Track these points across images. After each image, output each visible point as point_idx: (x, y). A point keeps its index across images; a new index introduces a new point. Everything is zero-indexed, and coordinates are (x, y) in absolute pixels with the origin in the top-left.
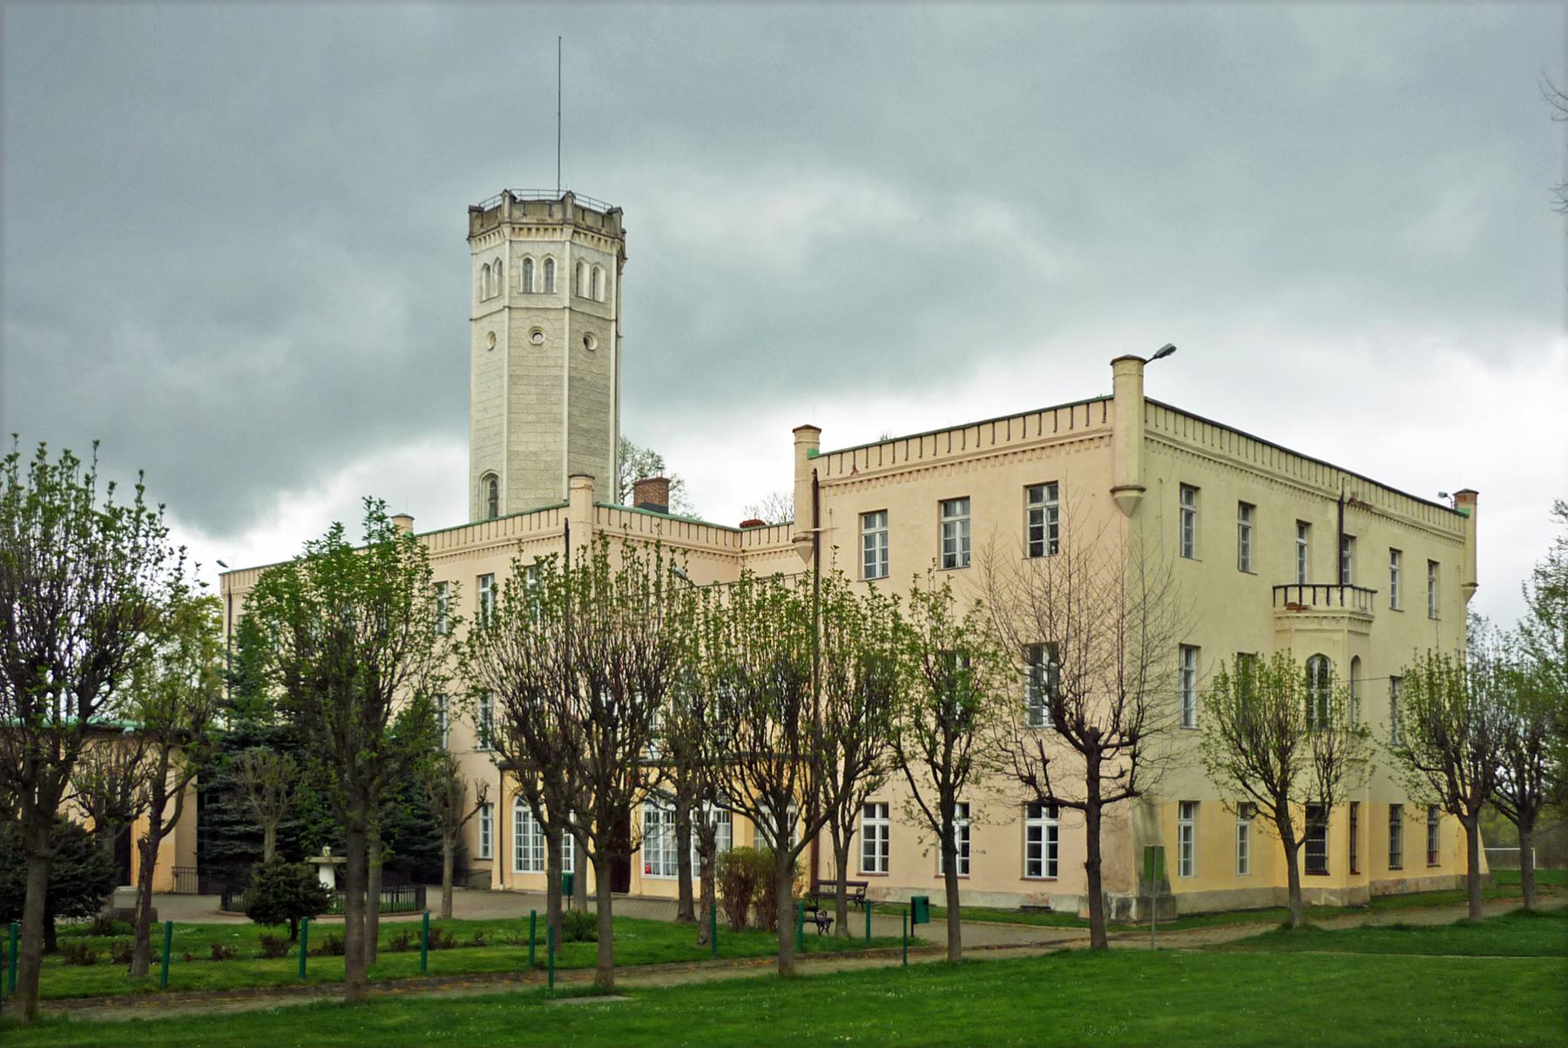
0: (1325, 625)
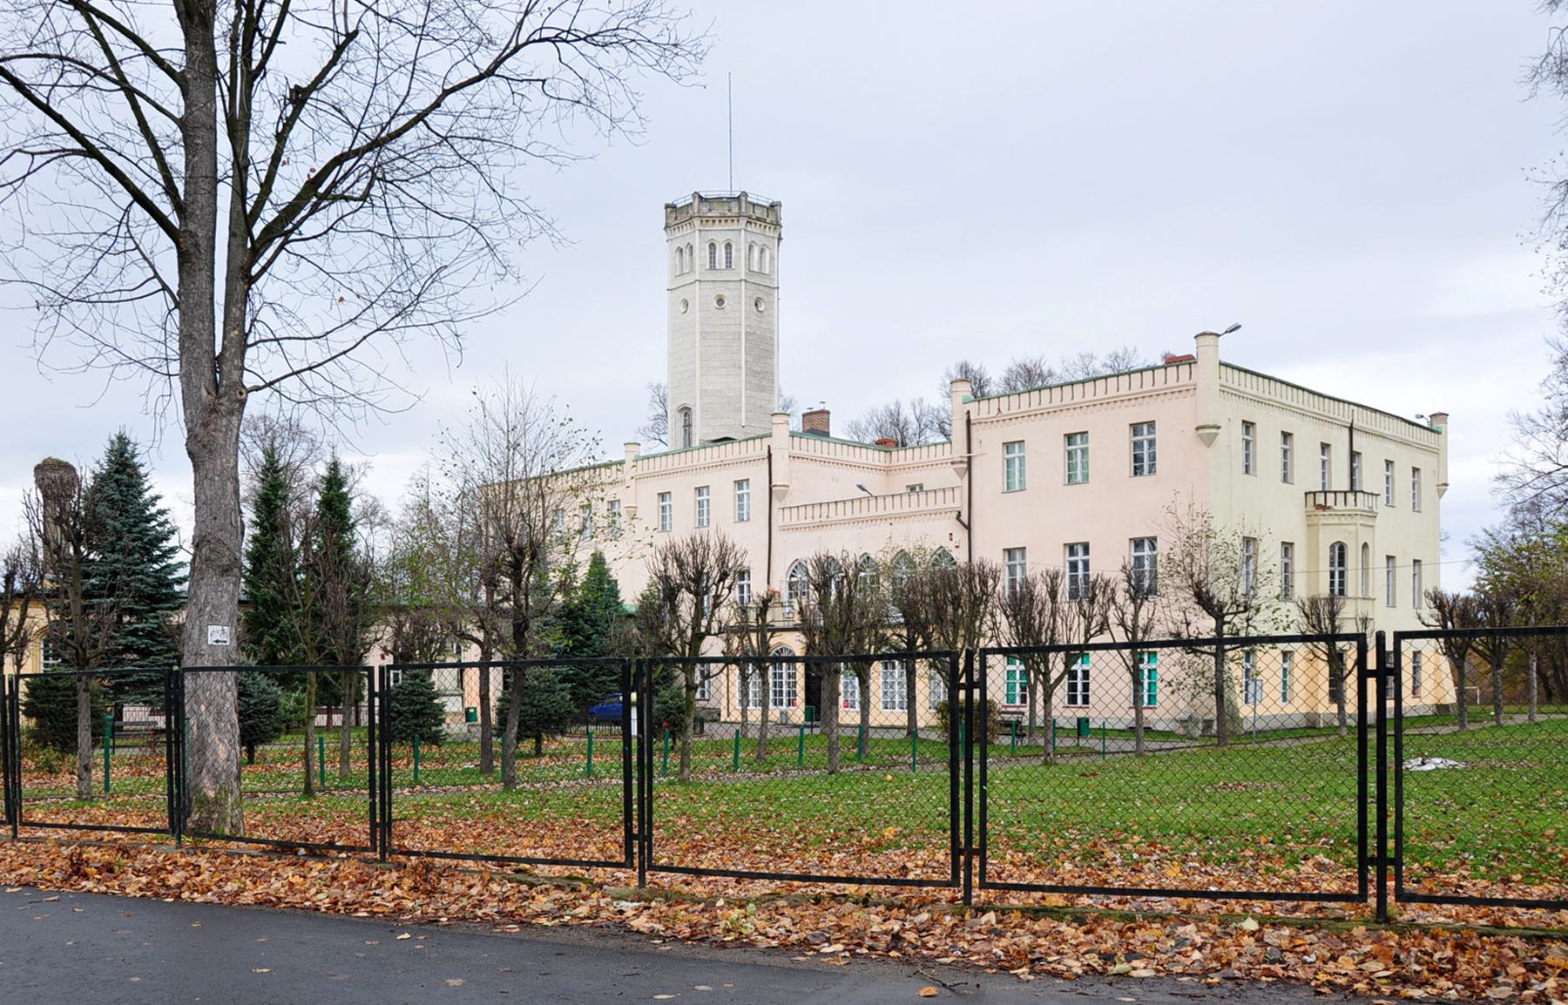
0: (1343, 520)
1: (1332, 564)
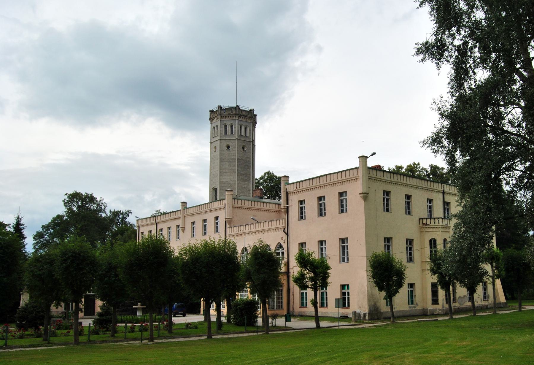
0: (434, 230)
1: (431, 247)
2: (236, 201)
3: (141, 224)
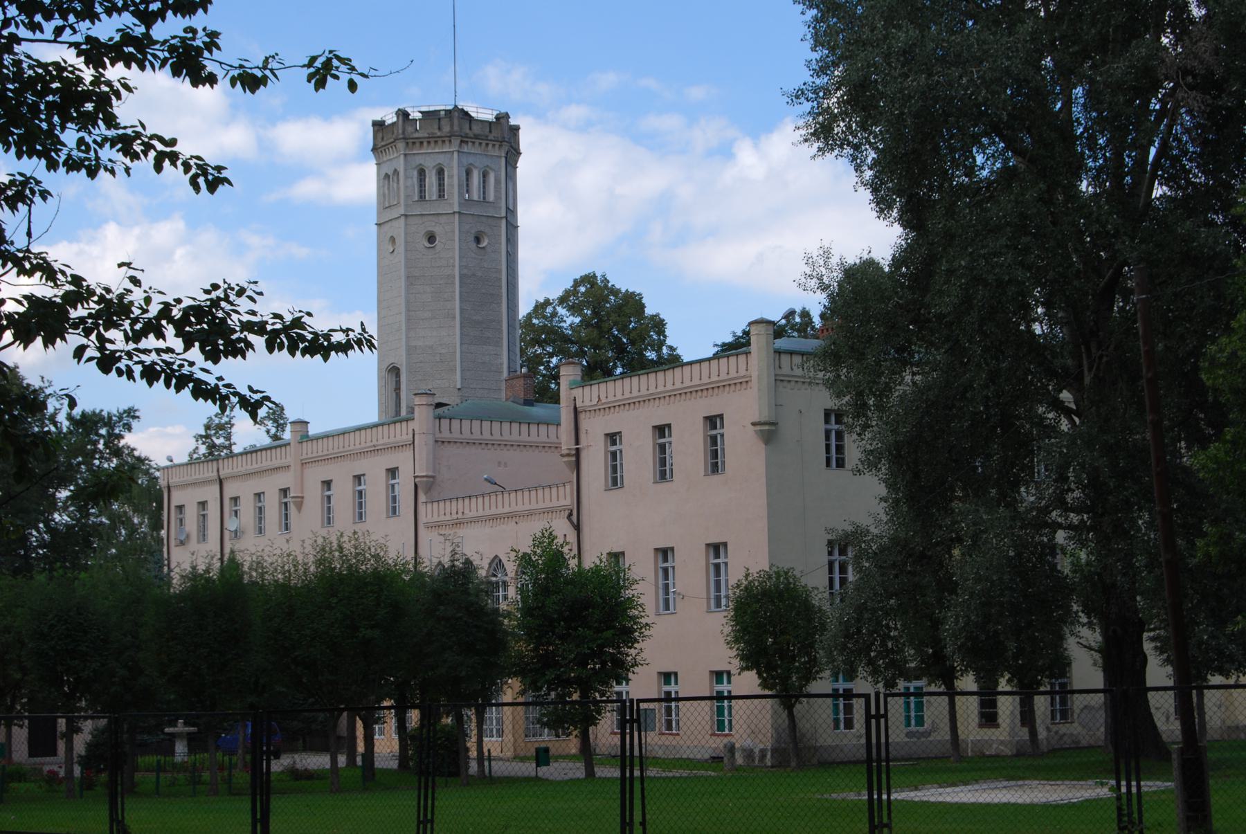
2: (445, 422)
3: (174, 480)
